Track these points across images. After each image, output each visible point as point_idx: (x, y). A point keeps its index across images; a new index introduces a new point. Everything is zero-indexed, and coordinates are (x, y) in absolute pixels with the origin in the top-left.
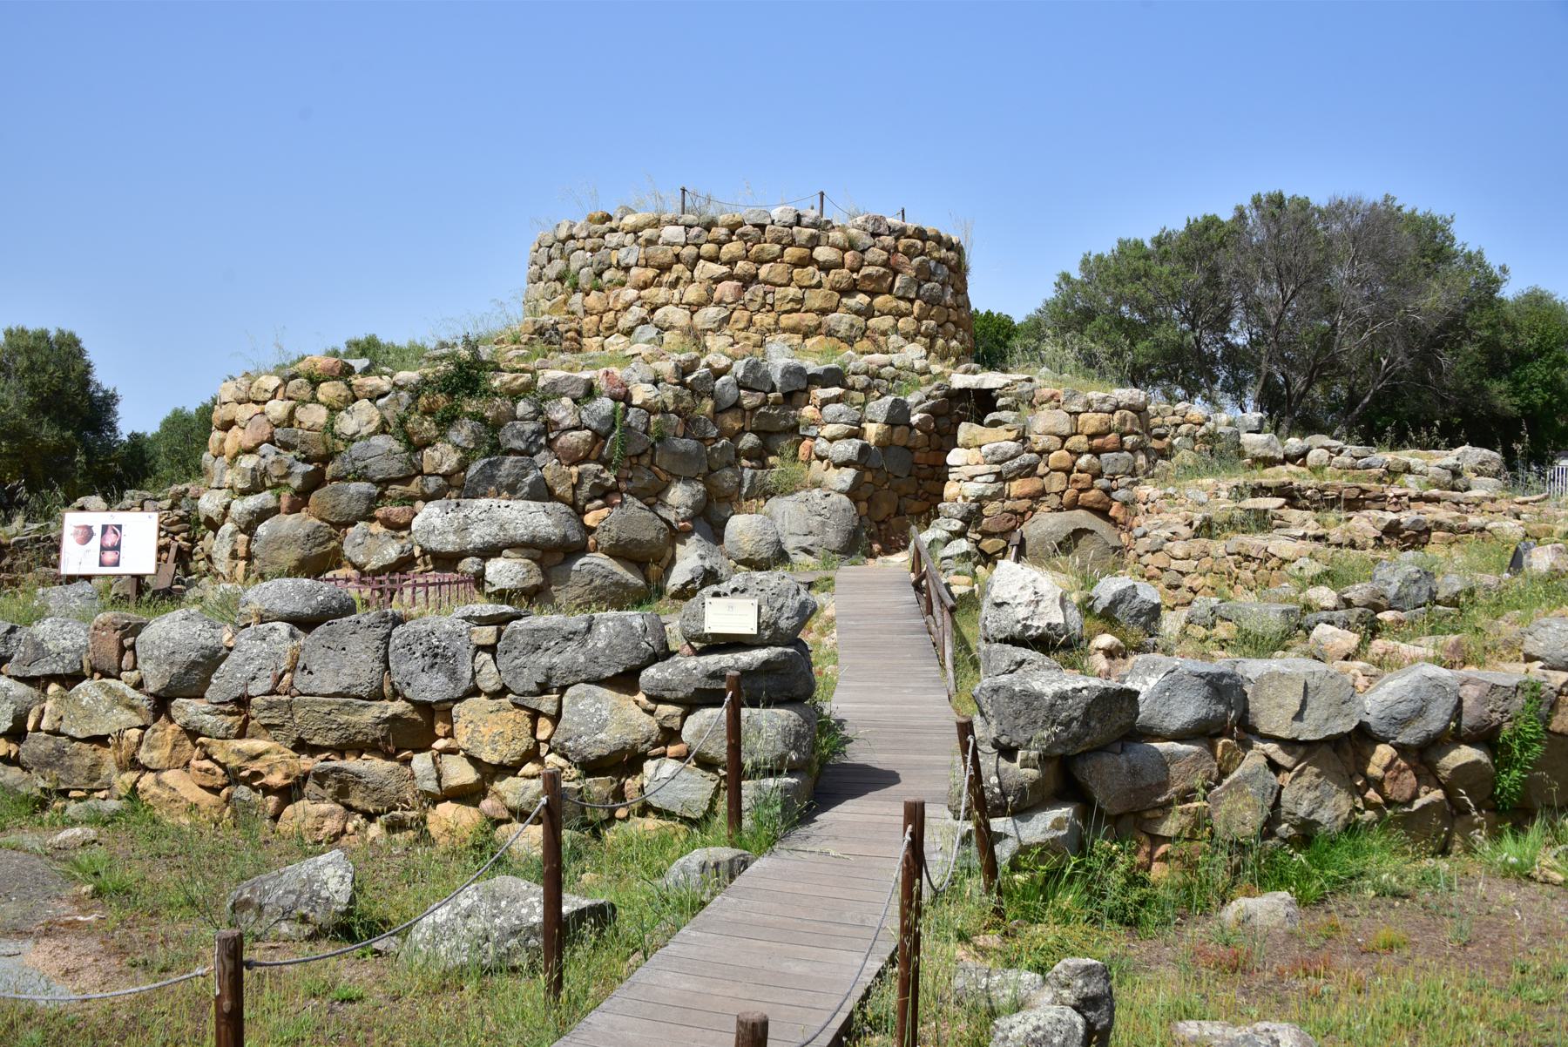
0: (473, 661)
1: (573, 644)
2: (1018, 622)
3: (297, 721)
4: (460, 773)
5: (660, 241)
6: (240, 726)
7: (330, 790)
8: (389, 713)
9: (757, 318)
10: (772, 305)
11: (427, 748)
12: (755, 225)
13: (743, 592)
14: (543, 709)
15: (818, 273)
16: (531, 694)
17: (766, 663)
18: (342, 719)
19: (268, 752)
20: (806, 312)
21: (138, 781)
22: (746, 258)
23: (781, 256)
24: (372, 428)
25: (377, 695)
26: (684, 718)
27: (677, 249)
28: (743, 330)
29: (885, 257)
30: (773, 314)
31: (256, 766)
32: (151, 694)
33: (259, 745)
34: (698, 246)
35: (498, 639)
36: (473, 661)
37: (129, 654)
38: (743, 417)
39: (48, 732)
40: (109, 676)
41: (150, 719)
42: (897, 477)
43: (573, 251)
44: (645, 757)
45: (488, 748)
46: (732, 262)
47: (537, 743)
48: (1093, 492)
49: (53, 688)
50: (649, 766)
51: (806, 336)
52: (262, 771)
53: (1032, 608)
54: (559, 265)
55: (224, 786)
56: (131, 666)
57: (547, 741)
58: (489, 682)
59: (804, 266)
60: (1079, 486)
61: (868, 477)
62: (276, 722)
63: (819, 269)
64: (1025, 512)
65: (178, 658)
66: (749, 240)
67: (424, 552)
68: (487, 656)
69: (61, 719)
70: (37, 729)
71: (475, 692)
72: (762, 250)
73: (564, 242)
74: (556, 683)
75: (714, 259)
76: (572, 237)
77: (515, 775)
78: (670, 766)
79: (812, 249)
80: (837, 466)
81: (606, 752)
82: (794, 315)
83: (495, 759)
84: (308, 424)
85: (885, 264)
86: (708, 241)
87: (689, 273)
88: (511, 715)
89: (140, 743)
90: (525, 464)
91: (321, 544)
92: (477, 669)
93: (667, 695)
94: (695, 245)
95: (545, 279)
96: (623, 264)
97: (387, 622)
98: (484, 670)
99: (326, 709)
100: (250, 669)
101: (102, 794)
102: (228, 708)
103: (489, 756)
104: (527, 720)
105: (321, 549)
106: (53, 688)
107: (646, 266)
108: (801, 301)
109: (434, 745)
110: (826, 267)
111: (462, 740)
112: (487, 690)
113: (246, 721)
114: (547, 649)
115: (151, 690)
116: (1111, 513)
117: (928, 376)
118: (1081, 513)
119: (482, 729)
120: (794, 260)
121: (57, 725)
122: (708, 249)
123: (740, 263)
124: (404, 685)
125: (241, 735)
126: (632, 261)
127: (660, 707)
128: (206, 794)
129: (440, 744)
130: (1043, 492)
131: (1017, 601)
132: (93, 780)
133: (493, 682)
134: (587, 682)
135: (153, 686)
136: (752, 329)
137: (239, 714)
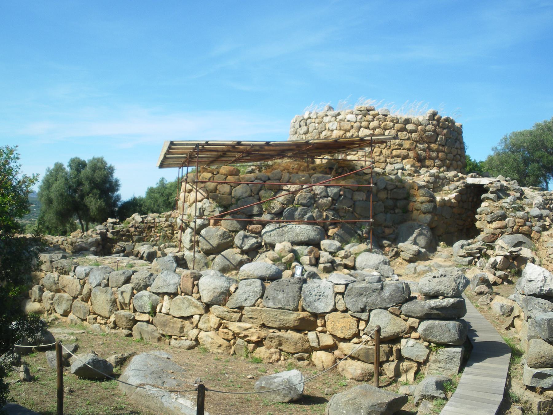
0: (335, 299)
1: (376, 294)
2: (538, 288)
3: (263, 317)
4: (327, 340)
5: (346, 120)
6: (240, 317)
7: (275, 344)
8: (301, 316)
9: (384, 151)
10: (390, 146)
11: (314, 330)
12: (383, 115)
13: (445, 276)
14: (363, 318)
15: (408, 134)
16: (358, 312)
17: (453, 304)
18: (282, 317)
19: (251, 328)
20: (403, 149)
21: (199, 334)
22: (379, 127)
23: (393, 127)
24: (247, 194)
25: (296, 309)
26: (419, 323)
27: (352, 124)
28: (378, 156)
29: (434, 129)
30: (390, 150)
31: (246, 333)
32: (205, 303)
33: (247, 325)
34: (361, 122)
35: (345, 291)
36: (335, 299)
37: (196, 287)
38: (388, 193)
39: (164, 314)
40: (188, 295)
41: (203, 312)
42: (446, 218)
43: (310, 123)
44: (402, 337)
45: (339, 332)
46: (374, 129)
47: (359, 330)
48: (525, 227)
49: (166, 297)
50: (403, 341)
51: (403, 159)
52: (249, 335)
53: (543, 283)
54: (304, 129)
55: (232, 339)
56: (196, 291)
57: (363, 330)
58: (341, 307)
59: (402, 132)
60: (520, 224)
61: (436, 218)
62: (254, 317)
63: (408, 133)
64: (499, 234)
65: (217, 291)
66: (381, 121)
67: (265, 244)
68: (341, 297)
69: (169, 309)
70: (160, 312)
71: (335, 310)
72: (386, 124)
73: (307, 120)
74: (368, 308)
75: (367, 128)
76: (310, 118)
77: (350, 342)
78: (411, 342)
79: (406, 125)
80: (424, 213)
81: (387, 335)
82: (398, 151)
83: (342, 336)
84: (222, 192)
85: (434, 131)
86: (364, 121)
87: (357, 133)
88: (349, 320)
89: (199, 321)
90: (305, 210)
91: (225, 239)
92: (336, 301)
93: (413, 315)
94: (360, 122)
95: (298, 133)
96: (330, 129)
97: (301, 282)
98: (339, 302)
99: (275, 313)
100: (245, 296)
101: (185, 338)
102: (235, 310)
103: (340, 335)
104: (356, 322)
105: (225, 241)
106: (166, 297)
107: (340, 129)
108: (401, 145)
109: (317, 329)
110: (411, 132)
111: (329, 327)
112: (340, 310)
113: (242, 315)
114: (365, 295)
115: (205, 301)
116: (531, 236)
117: (458, 178)
118: (520, 235)
119: (337, 324)
120: (399, 129)
121: (168, 311)
122: (364, 124)
123: (377, 130)
124: (307, 306)
125: (240, 320)
126: (334, 128)
127: (410, 318)
128: (225, 341)
129: (320, 329)
130: (505, 227)
131: (537, 280)
132: (181, 333)
133: (343, 307)
134: (380, 308)
135: (206, 299)
136: (382, 156)
137: (239, 312)
